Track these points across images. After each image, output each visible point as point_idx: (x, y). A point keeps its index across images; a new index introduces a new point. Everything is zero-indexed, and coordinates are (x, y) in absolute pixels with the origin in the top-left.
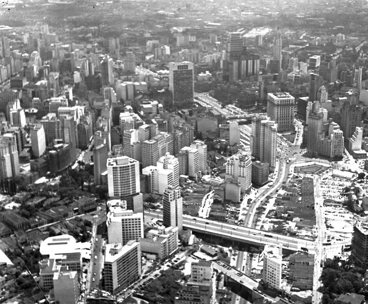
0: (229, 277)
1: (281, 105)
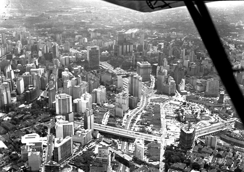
0: (117, 155)
1: (144, 68)
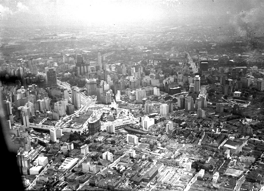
0: (39, 140)
1: (90, 84)
